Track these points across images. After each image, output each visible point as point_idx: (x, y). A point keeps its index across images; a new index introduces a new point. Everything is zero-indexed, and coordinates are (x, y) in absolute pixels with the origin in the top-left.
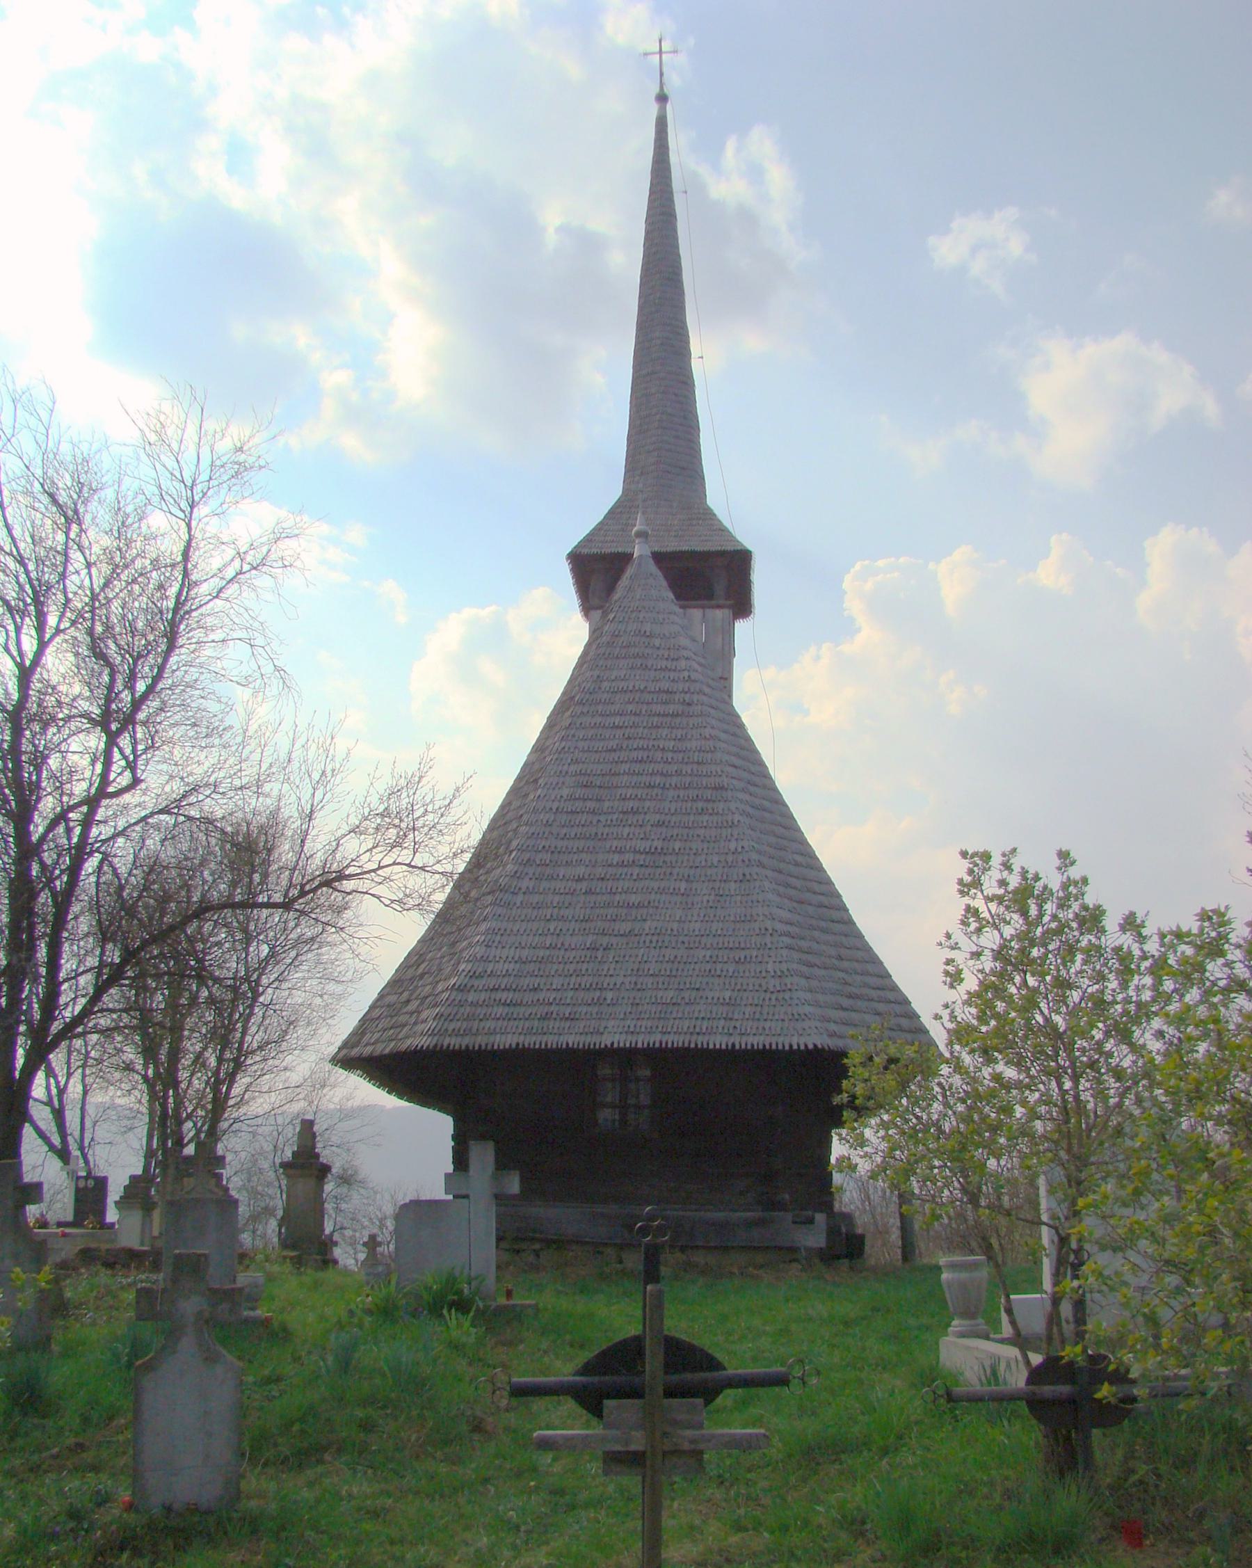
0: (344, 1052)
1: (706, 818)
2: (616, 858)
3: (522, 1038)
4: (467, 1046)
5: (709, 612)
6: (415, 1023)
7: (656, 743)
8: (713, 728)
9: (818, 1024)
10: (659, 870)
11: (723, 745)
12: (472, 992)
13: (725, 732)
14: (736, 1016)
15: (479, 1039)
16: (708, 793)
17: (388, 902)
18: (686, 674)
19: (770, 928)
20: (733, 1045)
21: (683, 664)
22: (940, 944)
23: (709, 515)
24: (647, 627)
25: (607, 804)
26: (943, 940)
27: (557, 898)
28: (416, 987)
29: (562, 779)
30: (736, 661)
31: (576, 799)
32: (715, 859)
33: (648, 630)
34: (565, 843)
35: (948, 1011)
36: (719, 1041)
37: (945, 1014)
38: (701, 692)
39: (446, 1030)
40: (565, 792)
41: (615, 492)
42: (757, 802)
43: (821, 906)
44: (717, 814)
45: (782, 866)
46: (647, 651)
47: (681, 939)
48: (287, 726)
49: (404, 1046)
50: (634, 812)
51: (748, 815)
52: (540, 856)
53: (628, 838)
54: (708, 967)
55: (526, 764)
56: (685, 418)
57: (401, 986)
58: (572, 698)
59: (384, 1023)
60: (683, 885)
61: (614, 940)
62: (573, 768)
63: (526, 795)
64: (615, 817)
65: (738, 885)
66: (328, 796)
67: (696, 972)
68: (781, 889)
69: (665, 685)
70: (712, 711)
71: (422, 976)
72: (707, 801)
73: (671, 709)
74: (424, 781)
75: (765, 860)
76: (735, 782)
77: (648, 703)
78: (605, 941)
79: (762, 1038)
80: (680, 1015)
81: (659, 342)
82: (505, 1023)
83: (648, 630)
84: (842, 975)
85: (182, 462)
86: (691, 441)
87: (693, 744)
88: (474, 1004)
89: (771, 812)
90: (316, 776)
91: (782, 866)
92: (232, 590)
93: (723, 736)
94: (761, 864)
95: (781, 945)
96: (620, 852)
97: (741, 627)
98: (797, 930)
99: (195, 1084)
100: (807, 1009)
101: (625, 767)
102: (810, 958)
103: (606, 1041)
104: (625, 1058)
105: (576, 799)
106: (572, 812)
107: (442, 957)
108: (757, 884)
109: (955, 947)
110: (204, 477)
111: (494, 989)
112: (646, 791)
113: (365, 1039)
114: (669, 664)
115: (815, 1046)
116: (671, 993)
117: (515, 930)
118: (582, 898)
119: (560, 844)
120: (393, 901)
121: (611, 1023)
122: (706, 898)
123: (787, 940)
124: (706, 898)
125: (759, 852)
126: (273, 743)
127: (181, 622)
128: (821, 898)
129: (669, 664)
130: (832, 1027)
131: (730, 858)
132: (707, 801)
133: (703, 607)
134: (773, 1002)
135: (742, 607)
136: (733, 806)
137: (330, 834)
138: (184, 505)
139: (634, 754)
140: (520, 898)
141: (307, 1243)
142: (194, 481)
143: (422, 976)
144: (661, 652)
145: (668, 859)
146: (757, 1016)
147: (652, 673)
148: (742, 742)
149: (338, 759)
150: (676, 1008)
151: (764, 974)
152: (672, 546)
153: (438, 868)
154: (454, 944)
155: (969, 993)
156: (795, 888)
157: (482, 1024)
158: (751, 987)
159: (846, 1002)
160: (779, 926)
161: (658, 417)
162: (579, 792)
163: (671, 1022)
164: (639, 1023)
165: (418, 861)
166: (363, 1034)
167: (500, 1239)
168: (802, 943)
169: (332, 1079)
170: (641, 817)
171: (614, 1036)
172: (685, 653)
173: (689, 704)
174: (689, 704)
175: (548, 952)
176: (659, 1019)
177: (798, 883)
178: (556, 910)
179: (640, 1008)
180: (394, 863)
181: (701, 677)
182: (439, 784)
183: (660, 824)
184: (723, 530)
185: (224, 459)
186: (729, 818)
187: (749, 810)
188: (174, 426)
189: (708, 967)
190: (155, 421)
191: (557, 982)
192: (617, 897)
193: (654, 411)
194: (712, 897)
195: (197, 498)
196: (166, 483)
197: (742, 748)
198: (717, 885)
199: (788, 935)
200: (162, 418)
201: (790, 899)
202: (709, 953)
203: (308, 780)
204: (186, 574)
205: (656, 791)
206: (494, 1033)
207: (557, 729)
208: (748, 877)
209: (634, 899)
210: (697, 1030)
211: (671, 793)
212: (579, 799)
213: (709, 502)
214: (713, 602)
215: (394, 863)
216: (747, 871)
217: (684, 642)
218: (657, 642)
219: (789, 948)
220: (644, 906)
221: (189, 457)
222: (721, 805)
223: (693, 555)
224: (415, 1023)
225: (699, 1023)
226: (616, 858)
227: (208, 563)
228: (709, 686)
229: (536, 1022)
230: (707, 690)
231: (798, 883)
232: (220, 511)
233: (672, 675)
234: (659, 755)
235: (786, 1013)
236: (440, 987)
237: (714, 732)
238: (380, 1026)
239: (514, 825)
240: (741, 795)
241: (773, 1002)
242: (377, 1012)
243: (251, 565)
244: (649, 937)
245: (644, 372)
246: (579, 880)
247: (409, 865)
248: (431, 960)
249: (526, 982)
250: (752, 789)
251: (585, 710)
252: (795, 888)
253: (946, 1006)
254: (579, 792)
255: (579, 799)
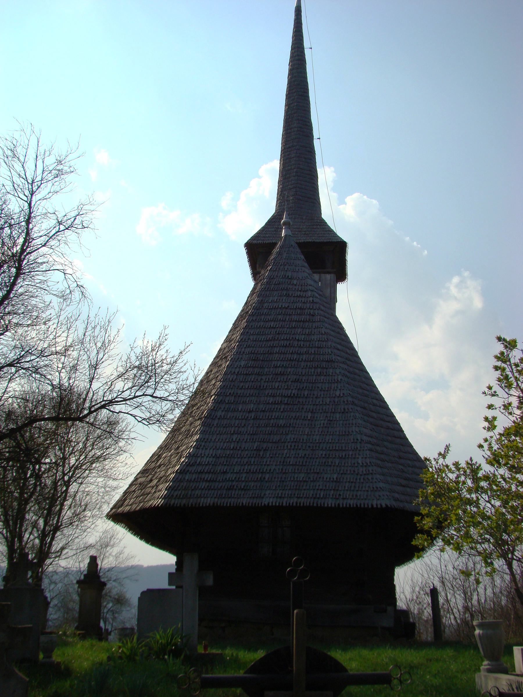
0: (114, 510)
1: (322, 377)
2: (271, 400)
3: (216, 500)
4: (184, 505)
5: (323, 275)
6: (155, 492)
7: (294, 337)
8: (326, 328)
9: (388, 494)
10: (295, 407)
11: (332, 338)
12: (188, 474)
13: (333, 331)
14: (340, 488)
15: (191, 501)
16: (324, 364)
17: (140, 419)
18: (311, 299)
19: (359, 439)
20: (339, 505)
21: (309, 293)
22: (484, 393)
23: (323, 223)
24: (289, 274)
25: (266, 370)
26: (486, 390)
27: (237, 422)
28: (156, 473)
29: (241, 356)
30: (337, 304)
31: (248, 367)
32: (328, 400)
33: (290, 275)
34: (243, 391)
35: (487, 443)
36: (330, 503)
37: (486, 445)
38: (319, 309)
39: (173, 495)
40: (243, 363)
41: (271, 210)
42: (351, 369)
43: (388, 428)
44: (329, 375)
45: (366, 405)
46: (289, 286)
47: (308, 444)
48: (84, 317)
49: (148, 505)
50: (282, 374)
51: (346, 376)
52: (228, 398)
53: (278, 388)
54: (324, 460)
55: (220, 350)
56: (310, 171)
57: (147, 473)
58: (247, 312)
59: (138, 493)
60: (310, 415)
61: (270, 445)
62: (247, 350)
63: (221, 365)
64: (271, 377)
65: (341, 414)
66: (106, 356)
67: (317, 463)
68: (366, 418)
69: (299, 305)
70: (326, 319)
71: (159, 466)
72: (323, 368)
73: (303, 318)
74: (162, 347)
75: (356, 402)
76: (339, 358)
77: (290, 315)
78: (265, 445)
79: (355, 501)
80: (308, 487)
81: (296, 129)
82: (207, 492)
83: (290, 275)
84: (401, 467)
85: (26, 168)
86: (314, 183)
87: (315, 337)
88: (189, 481)
89: (360, 376)
90: (99, 345)
91: (366, 405)
92: (52, 243)
93: (332, 333)
94: (353, 403)
95: (366, 448)
96: (274, 396)
97: (340, 286)
98: (375, 441)
99: (31, 538)
100: (381, 485)
101: (276, 350)
102: (382, 456)
103: (265, 501)
104: (275, 512)
105: (248, 367)
106: (246, 374)
107: (171, 455)
108: (352, 414)
109: (494, 395)
110: (39, 178)
111: (201, 473)
112: (289, 362)
113: (126, 503)
114: (302, 294)
115: (386, 505)
116: (302, 475)
117: (213, 439)
118: (252, 422)
119: (239, 392)
120: (144, 419)
121: (268, 492)
122: (322, 422)
123: (370, 446)
124: (322, 422)
125: (352, 397)
126: (75, 326)
127: (24, 259)
128: (389, 424)
129: (302, 294)
130: (396, 495)
131: (336, 400)
132: (323, 368)
133: (320, 273)
134: (362, 480)
135: (342, 276)
136: (338, 371)
137: (108, 377)
138: (27, 193)
139: (282, 343)
140: (216, 422)
141: (89, 622)
142: (33, 181)
143: (159, 466)
144: (297, 287)
145: (301, 400)
146: (352, 488)
147: (292, 299)
148: (343, 337)
149: (112, 335)
150: (305, 483)
151: (356, 465)
152: (303, 239)
153: (170, 398)
154: (178, 448)
155: (500, 434)
156: (372, 417)
157: (193, 492)
158: (349, 472)
159: (404, 482)
160: (365, 438)
161: (295, 170)
162: (250, 363)
163: (303, 491)
164: (284, 492)
165: (158, 394)
166: (125, 500)
167: (201, 620)
168: (378, 448)
169: (112, 543)
170: (285, 377)
171: (269, 499)
172: (311, 288)
173: (313, 315)
174: (313, 315)
175: (232, 452)
176: (296, 489)
177: (374, 415)
178: (237, 429)
179: (285, 483)
180: (143, 395)
181: (319, 301)
182: (171, 349)
183: (295, 381)
184: (330, 231)
185: (51, 168)
186: (336, 378)
187: (348, 374)
188: (21, 147)
189: (324, 460)
190: (10, 144)
191: (237, 469)
192: (272, 421)
193: (293, 167)
194: (326, 421)
195: (34, 189)
196: (16, 179)
197: (343, 340)
198: (329, 415)
199: (369, 443)
200: (15, 143)
201: (371, 423)
202: (324, 453)
203: (94, 347)
204: (28, 234)
205: (294, 363)
206: (200, 497)
207: (238, 329)
208: (347, 410)
209: (282, 422)
210: (318, 496)
211: (303, 364)
212: (250, 367)
213: (322, 216)
214: (325, 270)
215: (143, 395)
216: (346, 407)
217: (310, 282)
218: (295, 282)
219: (371, 450)
220: (287, 427)
221: (30, 166)
222: (331, 371)
223: (313, 244)
224: (155, 492)
225: (319, 492)
226: (271, 400)
227: (41, 227)
228: (324, 306)
229: (225, 492)
230: (322, 308)
231: (374, 415)
232: (48, 196)
233: (303, 299)
234: (296, 343)
235: (369, 487)
236: (169, 472)
237: (327, 331)
238: (135, 495)
239: (213, 382)
240: (341, 365)
241: (362, 480)
242: (133, 488)
243: (65, 226)
244: (290, 444)
245: (288, 146)
246: (250, 412)
247: (152, 396)
248: (165, 458)
249: (219, 468)
250: (348, 362)
251: (254, 319)
252: (372, 417)
253: (486, 440)
254: (250, 363)
255: (250, 367)
